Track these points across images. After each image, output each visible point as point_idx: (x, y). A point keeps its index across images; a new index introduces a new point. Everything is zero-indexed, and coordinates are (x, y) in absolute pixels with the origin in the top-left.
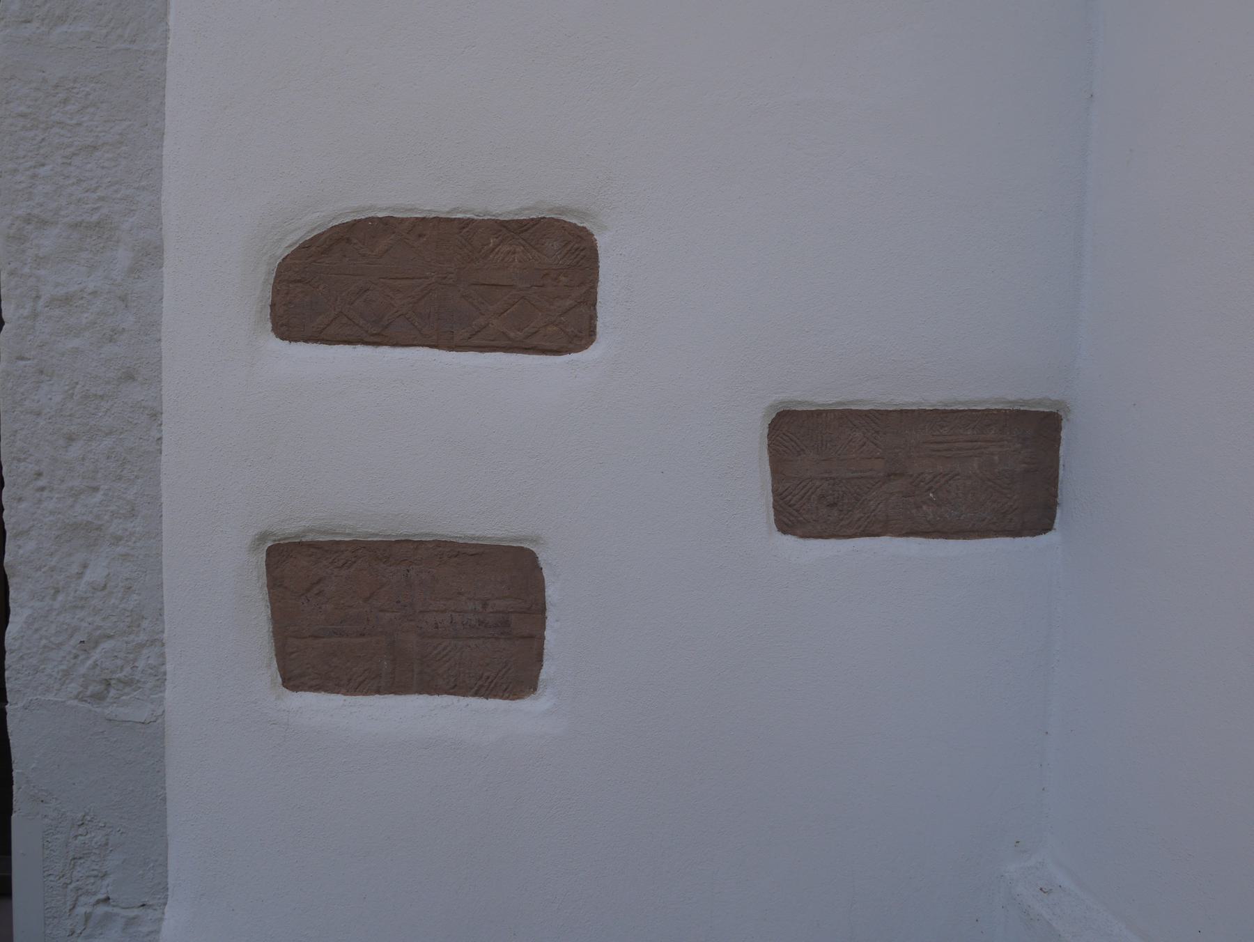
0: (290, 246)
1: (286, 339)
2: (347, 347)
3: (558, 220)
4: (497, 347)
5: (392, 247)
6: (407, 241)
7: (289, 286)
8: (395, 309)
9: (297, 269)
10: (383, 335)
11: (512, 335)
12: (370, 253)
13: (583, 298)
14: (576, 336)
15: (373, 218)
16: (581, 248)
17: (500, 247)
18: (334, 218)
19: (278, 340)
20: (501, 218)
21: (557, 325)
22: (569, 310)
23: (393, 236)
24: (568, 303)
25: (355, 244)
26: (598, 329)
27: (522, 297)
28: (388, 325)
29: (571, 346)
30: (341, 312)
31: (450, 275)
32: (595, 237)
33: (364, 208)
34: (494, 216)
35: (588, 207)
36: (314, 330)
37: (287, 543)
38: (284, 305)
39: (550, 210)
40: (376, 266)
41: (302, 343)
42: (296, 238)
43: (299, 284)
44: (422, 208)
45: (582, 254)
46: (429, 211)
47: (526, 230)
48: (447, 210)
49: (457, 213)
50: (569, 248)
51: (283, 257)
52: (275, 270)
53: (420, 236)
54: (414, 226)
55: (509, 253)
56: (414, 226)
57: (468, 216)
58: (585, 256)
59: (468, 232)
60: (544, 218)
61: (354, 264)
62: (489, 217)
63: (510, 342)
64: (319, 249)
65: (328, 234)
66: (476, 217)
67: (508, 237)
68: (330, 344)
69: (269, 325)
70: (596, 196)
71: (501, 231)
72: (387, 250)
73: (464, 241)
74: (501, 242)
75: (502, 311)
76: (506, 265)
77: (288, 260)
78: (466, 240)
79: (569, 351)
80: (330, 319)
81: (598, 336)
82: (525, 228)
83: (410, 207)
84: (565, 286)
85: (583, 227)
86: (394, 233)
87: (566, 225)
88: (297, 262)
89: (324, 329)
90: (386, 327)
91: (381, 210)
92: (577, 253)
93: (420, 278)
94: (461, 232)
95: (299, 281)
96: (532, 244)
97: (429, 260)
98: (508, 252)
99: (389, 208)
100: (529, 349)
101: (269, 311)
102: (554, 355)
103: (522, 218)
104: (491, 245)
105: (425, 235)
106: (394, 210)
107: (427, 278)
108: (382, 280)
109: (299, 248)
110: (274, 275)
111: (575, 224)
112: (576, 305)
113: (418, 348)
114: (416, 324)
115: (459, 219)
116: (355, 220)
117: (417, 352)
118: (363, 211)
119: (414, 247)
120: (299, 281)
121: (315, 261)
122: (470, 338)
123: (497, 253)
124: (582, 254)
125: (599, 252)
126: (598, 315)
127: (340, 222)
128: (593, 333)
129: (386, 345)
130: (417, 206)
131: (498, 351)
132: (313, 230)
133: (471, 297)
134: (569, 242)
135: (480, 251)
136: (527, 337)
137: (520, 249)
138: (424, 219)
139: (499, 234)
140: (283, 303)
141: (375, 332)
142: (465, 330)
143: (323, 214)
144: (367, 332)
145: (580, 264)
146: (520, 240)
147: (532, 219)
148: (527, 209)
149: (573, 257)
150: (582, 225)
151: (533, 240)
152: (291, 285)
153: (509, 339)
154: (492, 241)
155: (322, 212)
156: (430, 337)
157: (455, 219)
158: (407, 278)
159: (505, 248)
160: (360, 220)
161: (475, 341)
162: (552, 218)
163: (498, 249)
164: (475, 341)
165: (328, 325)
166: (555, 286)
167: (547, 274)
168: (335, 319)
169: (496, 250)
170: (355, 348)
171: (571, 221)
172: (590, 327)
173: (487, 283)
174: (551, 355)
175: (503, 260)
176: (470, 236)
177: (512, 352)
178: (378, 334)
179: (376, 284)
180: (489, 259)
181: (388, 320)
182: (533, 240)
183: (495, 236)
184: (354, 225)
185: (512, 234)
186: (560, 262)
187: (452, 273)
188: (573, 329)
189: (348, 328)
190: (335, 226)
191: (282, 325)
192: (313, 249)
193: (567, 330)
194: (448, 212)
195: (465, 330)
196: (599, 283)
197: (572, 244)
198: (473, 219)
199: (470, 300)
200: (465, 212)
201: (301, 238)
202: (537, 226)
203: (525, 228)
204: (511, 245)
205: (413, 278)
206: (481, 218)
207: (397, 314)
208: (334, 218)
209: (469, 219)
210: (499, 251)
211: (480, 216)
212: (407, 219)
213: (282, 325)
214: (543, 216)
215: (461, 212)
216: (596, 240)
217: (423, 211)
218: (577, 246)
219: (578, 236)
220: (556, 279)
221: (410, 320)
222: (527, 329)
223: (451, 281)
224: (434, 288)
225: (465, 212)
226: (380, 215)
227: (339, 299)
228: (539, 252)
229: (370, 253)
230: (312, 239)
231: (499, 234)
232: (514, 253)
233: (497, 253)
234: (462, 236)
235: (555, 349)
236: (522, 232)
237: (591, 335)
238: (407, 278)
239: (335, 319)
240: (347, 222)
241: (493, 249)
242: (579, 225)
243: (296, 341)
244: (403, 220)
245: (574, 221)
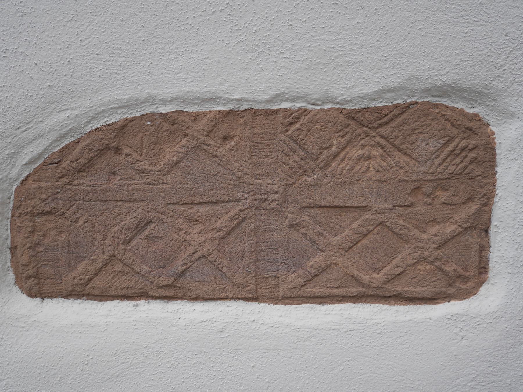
0: (30, 163)
1: (36, 297)
2: (125, 303)
3: (436, 106)
4: (344, 297)
5: (183, 158)
6: (206, 147)
7: (34, 222)
8: (192, 249)
9: (44, 196)
10: (176, 286)
11: (366, 278)
12: (151, 168)
13: (471, 221)
14: (459, 276)
15: (153, 114)
16: (471, 147)
17: (347, 150)
18: (93, 118)
19: (24, 297)
20: (349, 107)
21: (432, 262)
22: (449, 240)
23: (184, 142)
24: (450, 229)
25: (127, 155)
26: (491, 265)
27: (381, 223)
28: (183, 272)
29: (452, 290)
30: (113, 256)
31: (272, 195)
32: (493, 128)
33: (137, 100)
34: (338, 103)
35: (487, 83)
36: (75, 282)
37: (11, 234)
38: (30, 248)
39: (427, 91)
40: (161, 186)
41: (61, 300)
42: (39, 150)
43: (51, 217)
44: (227, 96)
45: (473, 155)
46: (238, 100)
47: (386, 123)
48: (266, 97)
49: (282, 101)
50: (450, 148)
51: (21, 179)
52: (12, 198)
53: (226, 138)
54: (216, 124)
55: (359, 160)
56: (216, 124)
57: (298, 105)
58: (475, 159)
59: (299, 129)
60: (416, 103)
61: (129, 185)
62: (330, 106)
63: (363, 289)
64: (74, 165)
65: (86, 143)
66: (310, 107)
67: (359, 135)
68: (100, 301)
69: (11, 276)
70: (501, 66)
71: (349, 125)
72: (177, 163)
73: (292, 144)
74: (349, 142)
75: (350, 244)
76: (356, 177)
77: (30, 182)
78: (295, 141)
79: (447, 297)
80: (98, 266)
81: (491, 274)
82: (385, 119)
83: (208, 96)
84: (444, 203)
85: (473, 114)
86: (186, 136)
87: (448, 113)
88: (43, 184)
89: (90, 280)
90: (181, 275)
91: (164, 102)
92: (463, 154)
93: (228, 202)
94: (287, 131)
95: (49, 213)
96: (396, 143)
97: (240, 174)
98: (360, 158)
99: (176, 99)
100: (390, 297)
101: (9, 256)
102: (425, 303)
103: (381, 105)
104: (334, 149)
105: (232, 138)
106: (184, 102)
107: (237, 201)
108: (171, 207)
109: (44, 164)
110: (11, 205)
111: (462, 111)
112: (460, 233)
113: (228, 303)
114: (225, 269)
115: (285, 110)
116: (126, 119)
117: (228, 309)
118: (137, 104)
119: (218, 157)
120: (49, 213)
121: (69, 183)
122: (302, 286)
123: (343, 160)
124: (473, 155)
125: (498, 151)
126: (492, 244)
127: (102, 123)
128: (483, 270)
129: (182, 298)
130: (220, 94)
131: (348, 302)
132: (62, 137)
133: (304, 227)
134: (452, 139)
135: (317, 159)
136: (388, 281)
137: (377, 152)
138: (230, 113)
139: (347, 130)
140: (28, 246)
141: (164, 283)
142: (296, 274)
143: (75, 112)
144: (152, 282)
145: (467, 171)
146: (378, 139)
147: (397, 106)
148: (390, 91)
149: (457, 160)
150: (471, 111)
151: (397, 137)
152: (37, 220)
153: (361, 284)
154: (335, 142)
155: (72, 109)
156: (246, 286)
157: (278, 110)
158: (209, 202)
159: (357, 152)
160: (133, 120)
161: (312, 290)
162: (429, 102)
163: (344, 153)
164: (312, 290)
165: (96, 275)
166: (429, 205)
167: (417, 188)
168: (105, 265)
169: (342, 155)
170: (137, 305)
171: (455, 105)
172: (480, 262)
173: (328, 205)
174: (430, 304)
175: (351, 170)
176: (301, 137)
177: (365, 302)
178: (169, 286)
179: (163, 213)
180: (330, 169)
181: (183, 265)
182: (397, 137)
183: (341, 134)
184: (124, 126)
185: (365, 129)
186: (439, 170)
187: (275, 193)
188: (455, 267)
189: (125, 277)
190: (96, 129)
191: (29, 277)
192: (65, 165)
193: (447, 269)
194: (268, 101)
195: (296, 274)
196: (496, 199)
197: (457, 140)
198: (305, 110)
199: (303, 231)
200: (294, 99)
201: (45, 150)
202: (405, 116)
203: (385, 119)
204: (363, 146)
205: (217, 203)
206: (319, 108)
207: (196, 256)
208: (93, 118)
209: (299, 109)
210: (345, 157)
211: (318, 105)
212: (205, 114)
213: (29, 277)
214: (413, 99)
215: (286, 100)
216: (493, 133)
217: (229, 101)
218: (463, 143)
219: (467, 128)
220: (431, 194)
221: (216, 263)
222: (387, 269)
223: (274, 205)
224: (250, 215)
225: (294, 99)
226: (163, 110)
227: (109, 236)
228: (405, 154)
229: (151, 168)
230: (62, 151)
231: (347, 130)
232: (369, 158)
233: (343, 160)
234: (291, 138)
235: (430, 297)
236: (380, 126)
237: (480, 273)
238: (209, 202)
239: (105, 265)
240: (113, 124)
241: (337, 155)
242: (468, 111)
243: (51, 297)
244: (198, 116)
245: (460, 105)
